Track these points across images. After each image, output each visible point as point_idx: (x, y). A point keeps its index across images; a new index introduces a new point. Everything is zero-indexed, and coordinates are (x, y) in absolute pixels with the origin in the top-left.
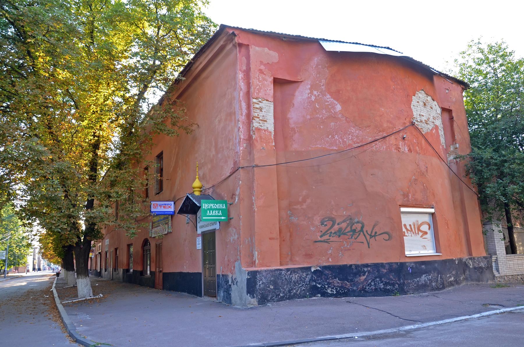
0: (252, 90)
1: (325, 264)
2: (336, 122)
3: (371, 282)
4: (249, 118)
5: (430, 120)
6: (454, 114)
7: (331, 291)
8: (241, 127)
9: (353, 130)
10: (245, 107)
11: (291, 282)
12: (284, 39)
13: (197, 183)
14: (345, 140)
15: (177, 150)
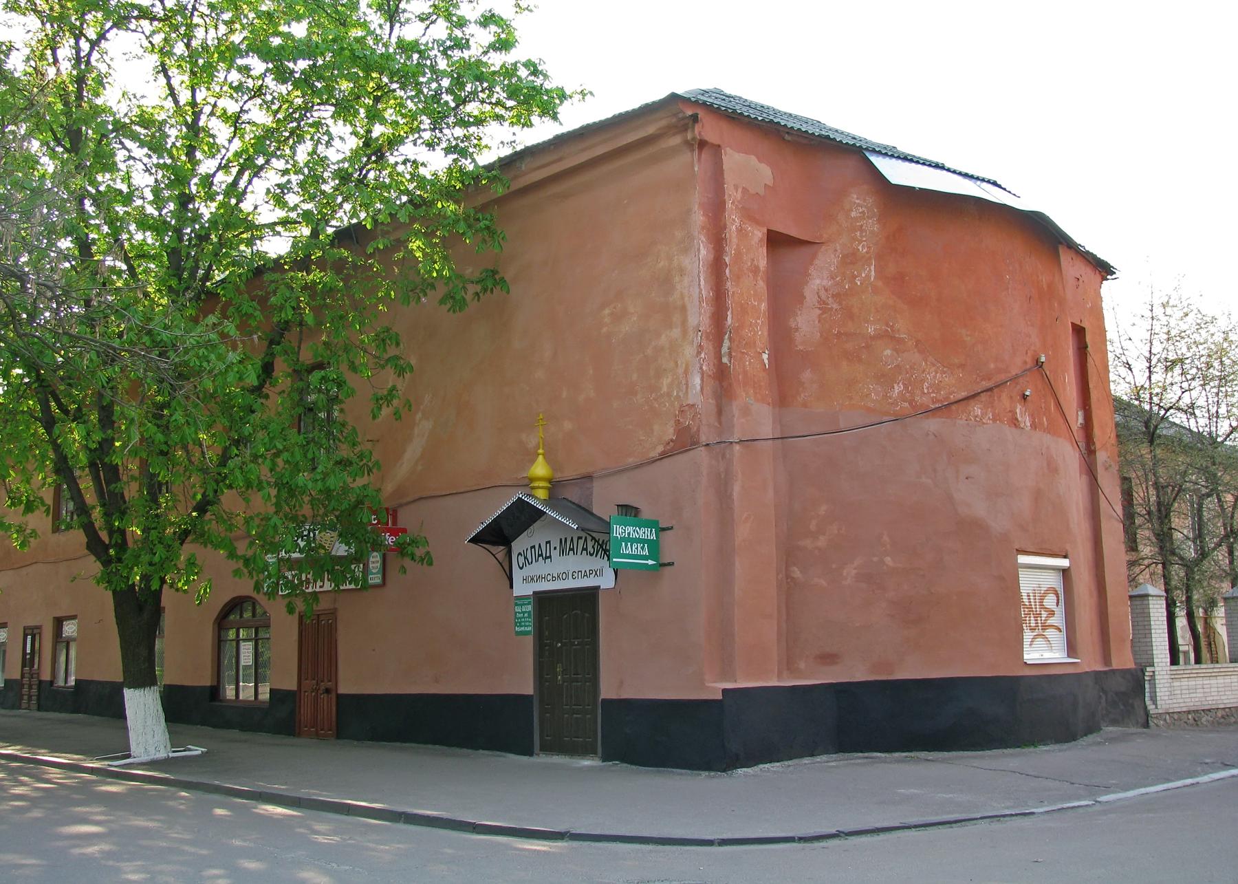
12: (787, 137)
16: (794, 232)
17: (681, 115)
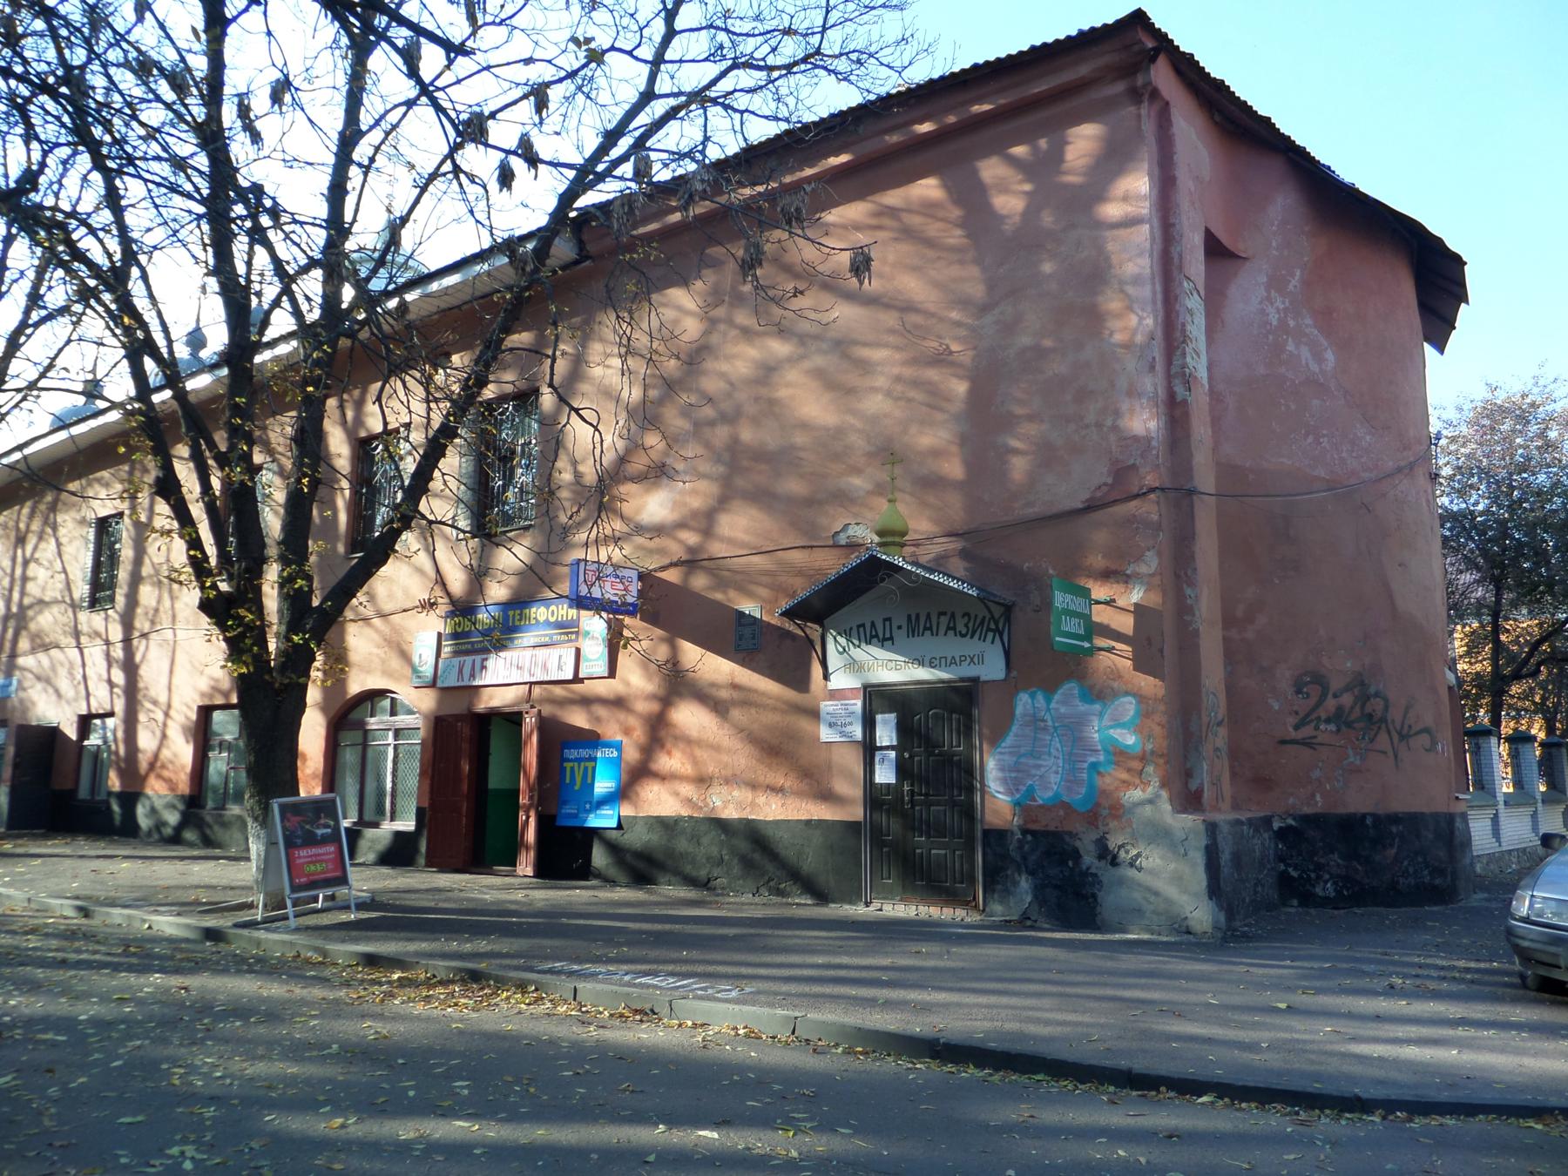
1: (1307, 810)
17: (1136, 48)
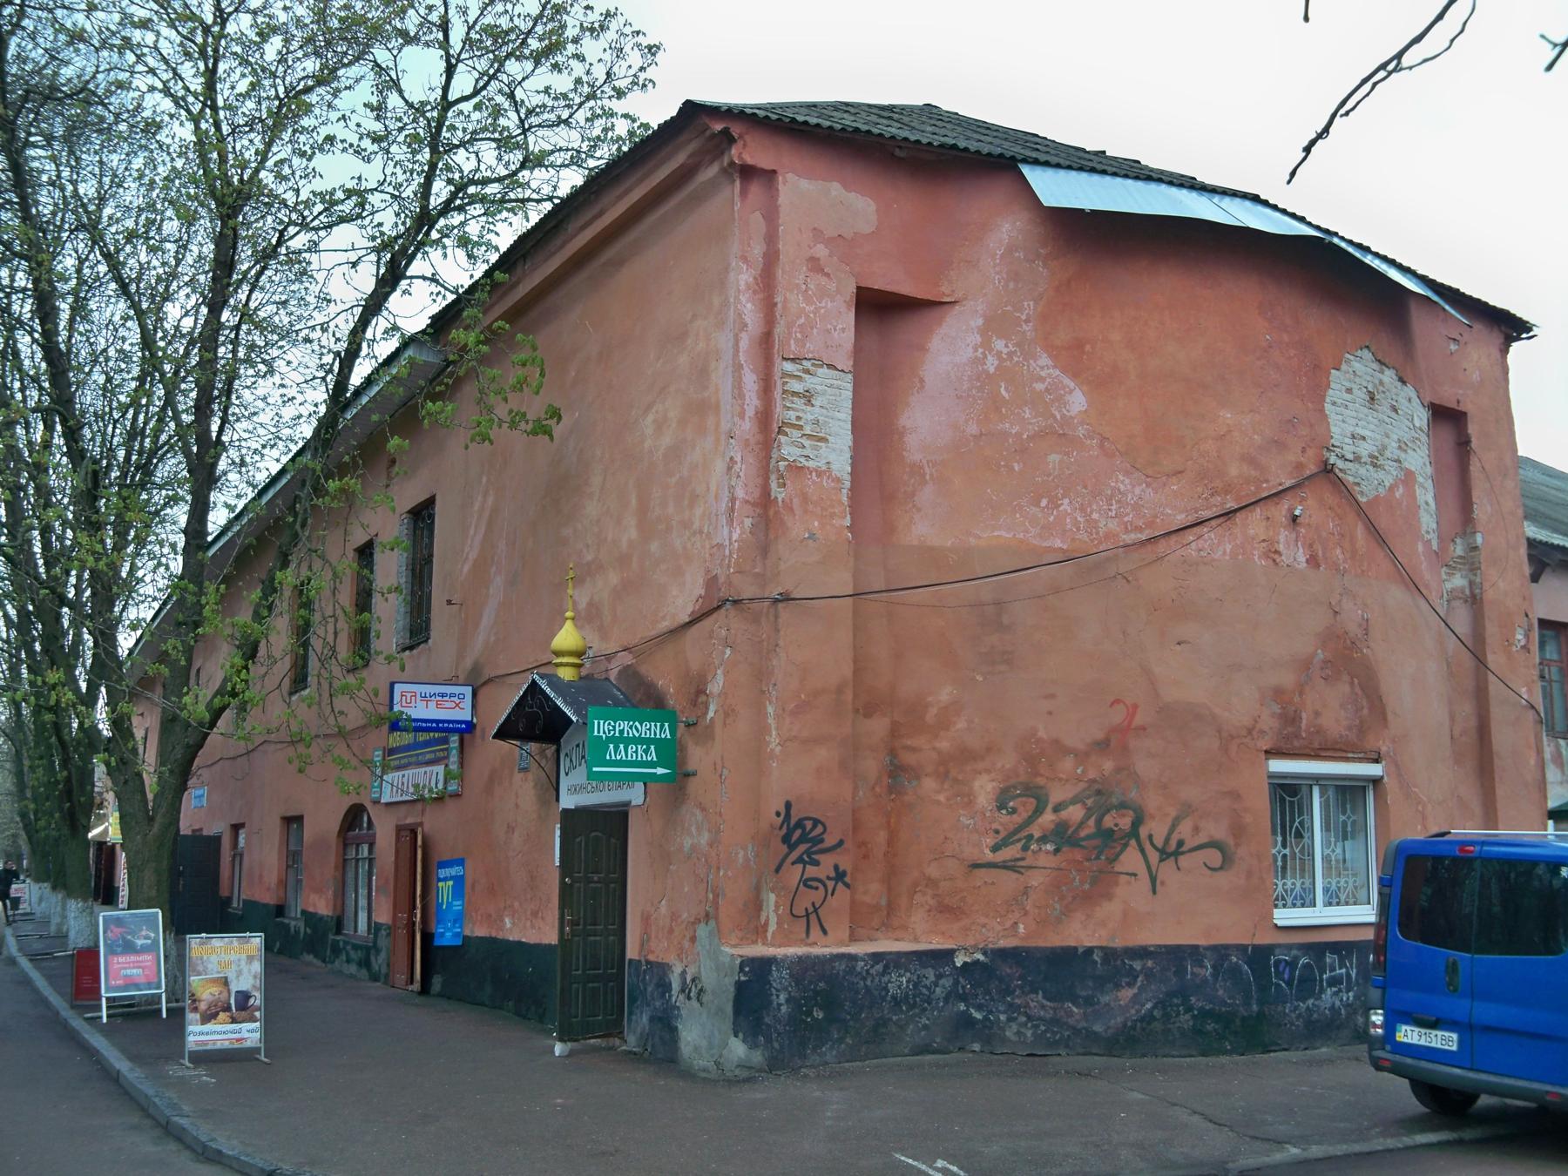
0: (779, 330)
1: (1002, 943)
2: (1067, 454)
3: (1154, 1007)
4: (768, 428)
5: (1388, 454)
6: (1472, 429)
7: (1018, 1033)
8: (738, 459)
9: (1123, 483)
10: (756, 387)
11: (883, 999)
12: (898, 152)
13: (567, 637)
14: (1095, 516)
15: (490, 500)
16: (906, 288)
17: (708, 133)
